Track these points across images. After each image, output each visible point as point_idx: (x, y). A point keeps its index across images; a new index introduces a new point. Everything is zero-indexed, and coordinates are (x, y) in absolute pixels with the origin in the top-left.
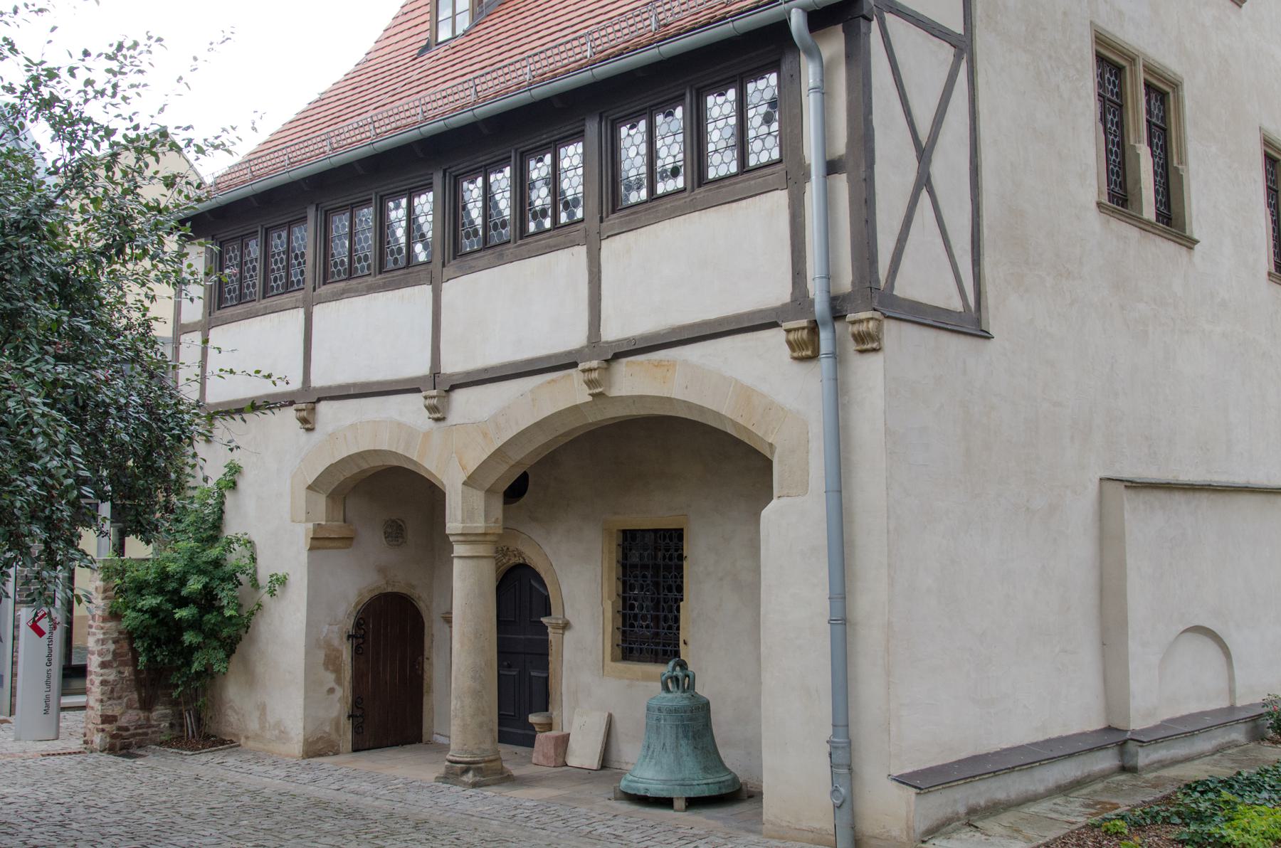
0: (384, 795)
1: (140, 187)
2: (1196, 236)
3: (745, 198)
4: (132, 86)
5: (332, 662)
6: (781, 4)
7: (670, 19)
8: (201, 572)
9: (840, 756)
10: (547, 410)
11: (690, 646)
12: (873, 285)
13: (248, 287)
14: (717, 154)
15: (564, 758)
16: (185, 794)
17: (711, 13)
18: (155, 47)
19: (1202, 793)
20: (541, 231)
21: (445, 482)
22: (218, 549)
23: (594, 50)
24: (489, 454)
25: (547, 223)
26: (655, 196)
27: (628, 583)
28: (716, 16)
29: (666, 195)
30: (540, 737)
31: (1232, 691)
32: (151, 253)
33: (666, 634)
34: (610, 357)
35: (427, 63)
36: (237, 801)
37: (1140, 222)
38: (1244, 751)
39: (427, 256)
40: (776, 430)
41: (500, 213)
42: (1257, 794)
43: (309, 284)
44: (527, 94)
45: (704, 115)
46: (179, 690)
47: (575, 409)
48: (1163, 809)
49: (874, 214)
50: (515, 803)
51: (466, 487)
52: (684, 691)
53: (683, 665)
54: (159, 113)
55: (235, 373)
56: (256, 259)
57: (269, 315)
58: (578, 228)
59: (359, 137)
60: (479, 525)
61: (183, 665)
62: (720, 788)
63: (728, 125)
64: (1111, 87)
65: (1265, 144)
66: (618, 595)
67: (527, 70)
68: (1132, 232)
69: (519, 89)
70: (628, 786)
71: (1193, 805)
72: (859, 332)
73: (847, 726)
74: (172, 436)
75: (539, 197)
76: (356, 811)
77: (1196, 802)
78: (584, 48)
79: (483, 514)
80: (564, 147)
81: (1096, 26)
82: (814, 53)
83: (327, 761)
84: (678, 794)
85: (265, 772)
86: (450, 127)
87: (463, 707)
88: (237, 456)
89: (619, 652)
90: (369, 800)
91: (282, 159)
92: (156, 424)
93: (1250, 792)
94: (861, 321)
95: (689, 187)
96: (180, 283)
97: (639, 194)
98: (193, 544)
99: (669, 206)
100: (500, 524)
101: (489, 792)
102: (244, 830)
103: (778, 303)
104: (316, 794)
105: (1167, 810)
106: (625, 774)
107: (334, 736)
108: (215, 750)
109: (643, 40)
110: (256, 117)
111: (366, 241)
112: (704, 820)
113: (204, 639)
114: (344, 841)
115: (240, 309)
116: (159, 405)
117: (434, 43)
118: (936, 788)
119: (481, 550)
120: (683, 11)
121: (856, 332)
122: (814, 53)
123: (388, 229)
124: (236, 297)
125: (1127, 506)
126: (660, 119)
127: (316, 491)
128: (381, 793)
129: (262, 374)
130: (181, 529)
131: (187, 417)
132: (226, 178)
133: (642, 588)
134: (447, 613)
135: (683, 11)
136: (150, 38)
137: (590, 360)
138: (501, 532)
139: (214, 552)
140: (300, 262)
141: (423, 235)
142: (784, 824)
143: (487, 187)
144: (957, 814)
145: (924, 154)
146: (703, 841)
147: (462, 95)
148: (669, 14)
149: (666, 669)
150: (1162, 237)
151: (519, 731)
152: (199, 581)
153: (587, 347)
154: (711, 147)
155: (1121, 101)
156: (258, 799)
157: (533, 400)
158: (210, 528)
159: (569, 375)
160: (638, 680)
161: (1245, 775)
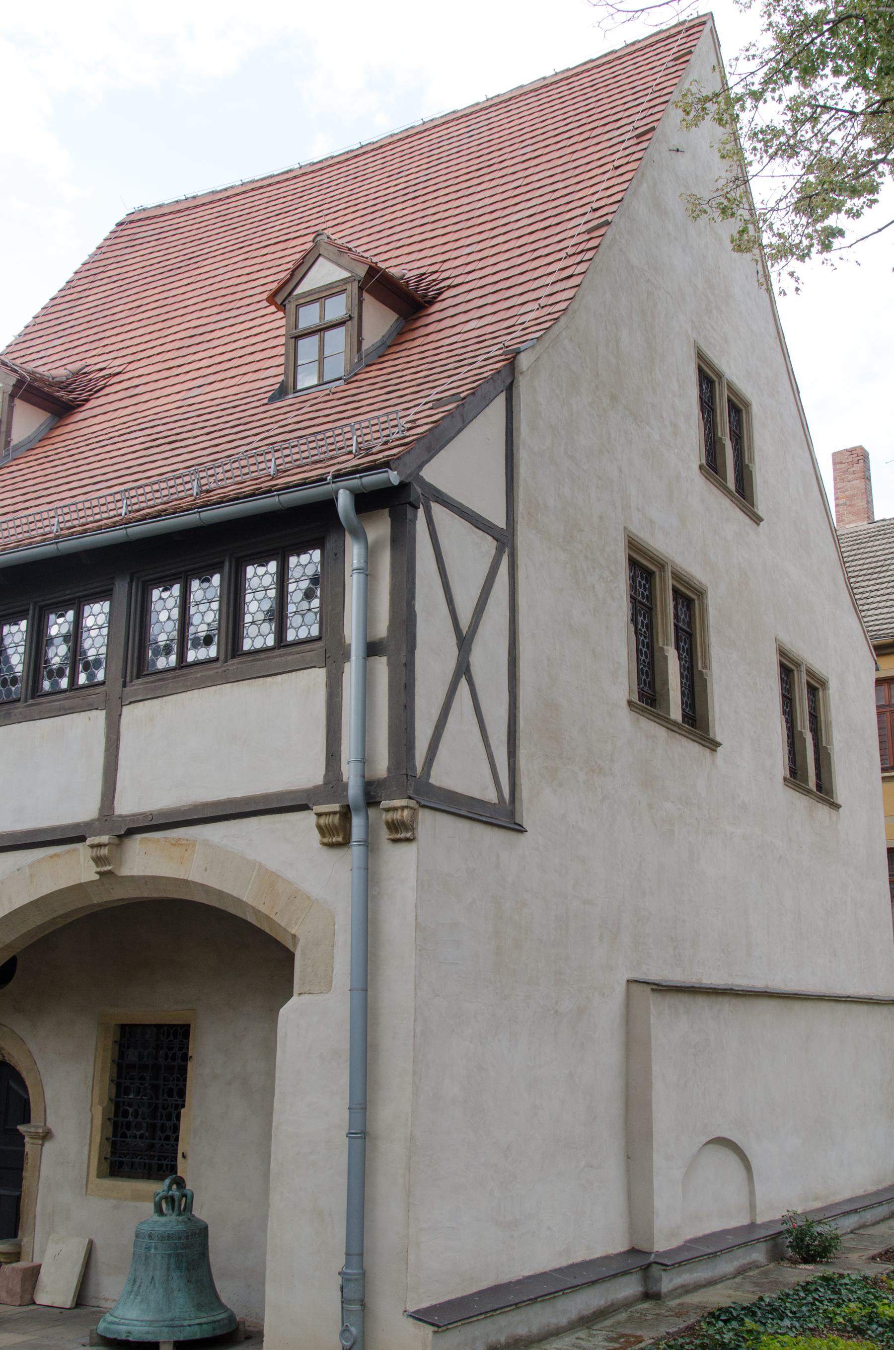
2: (719, 739)
3: (280, 674)
6: (329, 483)
7: (213, 486)
10: (46, 886)
12: (410, 773)
14: (254, 626)
15: (32, 1295)
17: (256, 484)
19: (726, 1322)
20: (56, 691)
23: (130, 508)
25: (64, 683)
26: (184, 664)
28: (261, 488)
29: (197, 664)
31: (752, 1206)
34: (122, 832)
37: (667, 722)
38: (766, 1274)
41: (11, 668)
42: (779, 1322)
44: (54, 547)
45: (243, 584)
47: (79, 888)
48: (688, 1341)
49: (414, 700)
52: (179, 1214)
53: (180, 1183)
58: (98, 691)
62: (214, 1329)
64: (641, 590)
65: (780, 654)
68: (660, 732)
69: (44, 540)
70: (106, 1329)
71: (717, 1337)
72: (393, 821)
73: (362, 1254)
75: (56, 655)
77: (720, 1332)
78: (119, 504)
80: (88, 604)
81: (630, 531)
82: (359, 534)
89: (106, 1166)
93: (772, 1319)
94: (395, 809)
95: (222, 658)
99: (199, 675)
103: (310, 785)
105: (692, 1342)
106: (105, 1313)
109: (184, 504)
118: (455, 1325)
120: (227, 479)
121: (390, 820)
122: (359, 534)
125: (653, 1009)
126: (195, 584)
133: (138, 1093)
135: (227, 479)
137: (100, 834)
145: (464, 642)
148: (212, 479)
149: (159, 1187)
150: (688, 738)
153: (98, 820)
154: (248, 618)
155: (651, 604)
157: (31, 876)
159: (75, 850)
160: (126, 1199)
161: (767, 1300)
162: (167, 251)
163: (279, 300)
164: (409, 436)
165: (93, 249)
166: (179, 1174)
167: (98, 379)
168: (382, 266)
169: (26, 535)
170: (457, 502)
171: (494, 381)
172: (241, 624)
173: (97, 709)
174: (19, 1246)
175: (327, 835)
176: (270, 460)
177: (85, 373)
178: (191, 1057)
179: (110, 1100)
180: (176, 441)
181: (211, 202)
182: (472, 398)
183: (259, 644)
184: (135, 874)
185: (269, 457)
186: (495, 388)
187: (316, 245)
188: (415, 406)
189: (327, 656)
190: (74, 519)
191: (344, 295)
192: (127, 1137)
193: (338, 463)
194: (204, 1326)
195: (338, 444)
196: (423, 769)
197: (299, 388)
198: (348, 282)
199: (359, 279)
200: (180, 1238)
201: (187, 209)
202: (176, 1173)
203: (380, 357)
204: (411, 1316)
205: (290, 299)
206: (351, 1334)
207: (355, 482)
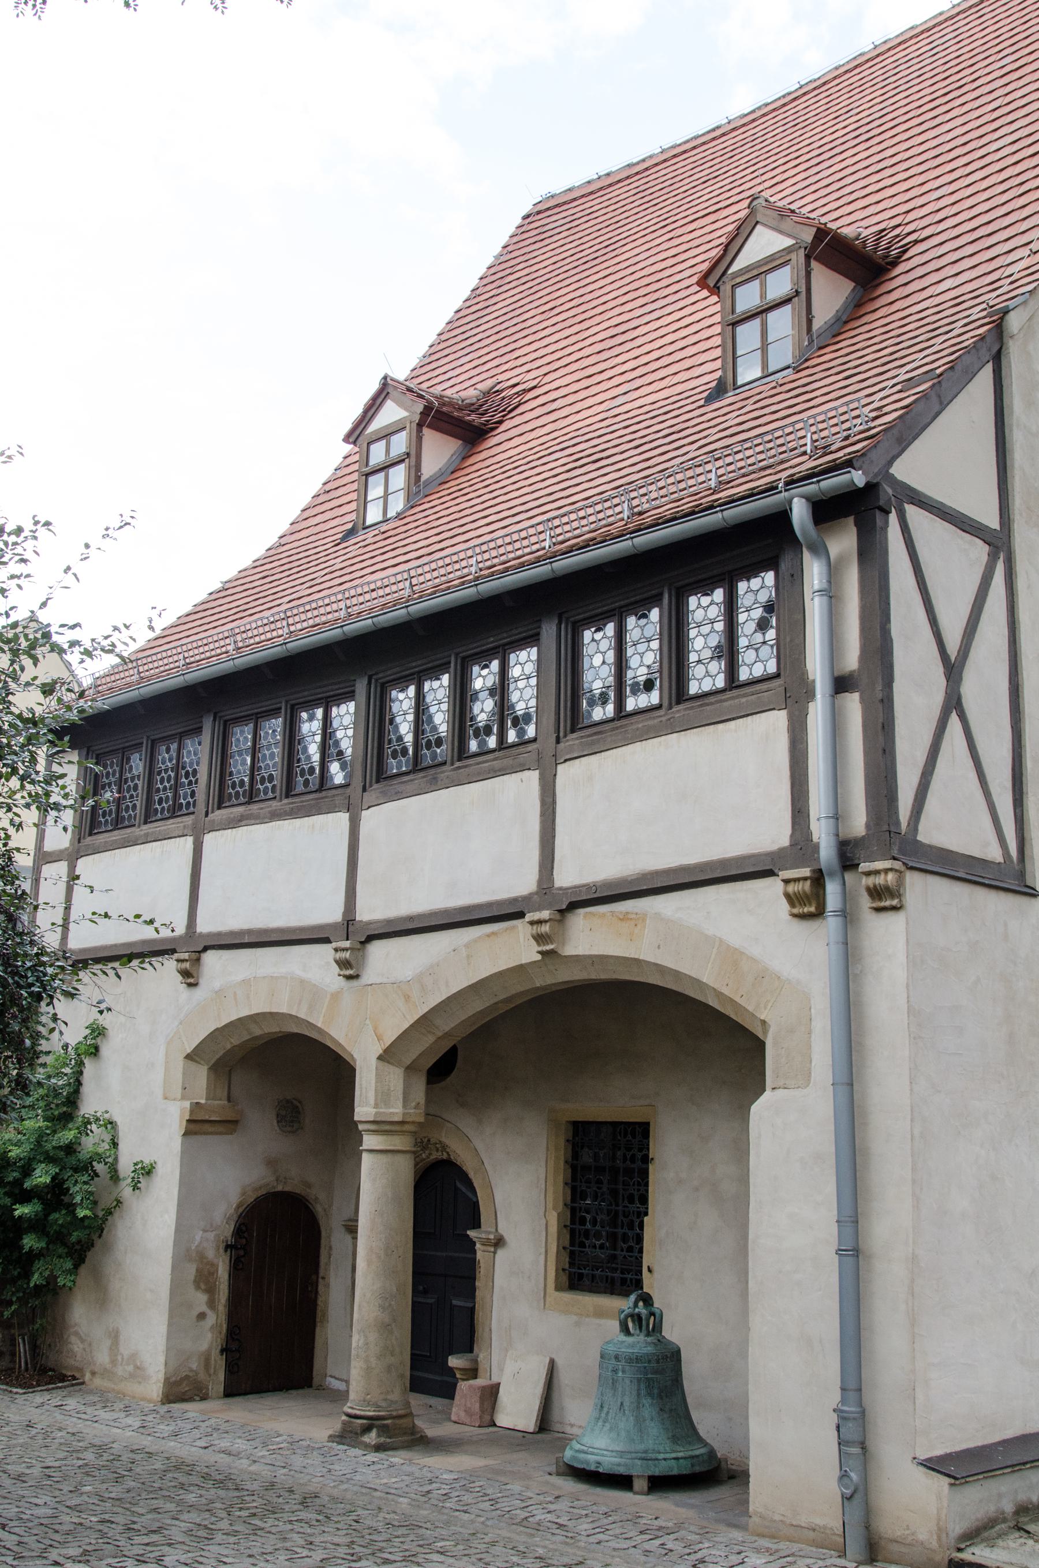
0: (263, 1457)
1: (12, 694)
3: (734, 719)
4: (12, 577)
5: (205, 1280)
6: (781, 492)
7: (646, 506)
8: (50, 1159)
9: (851, 1431)
10: (485, 969)
11: (656, 1274)
12: (893, 829)
13: (127, 810)
14: (700, 666)
16: (15, 1446)
18: (42, 532)
20: (484, 752)
22: (72, 1132)
23: (554, 540)
24: (412, 1022)
25: (492, 742)
26: (623, 714)
27: (579, 1190)
28: (701, 504)
30: (463, 1386)
32: (21, 772)
33: (625, 1257)
34: (564, 907)
35: (354, 551)
36: (78, 1459)
39: (345, 777)
40: (770, 1005)
41: (435, 728)
43: (201, 807)
44: (473, 590)
46: (13, 1308)
47: (520, 970)
50: (429, 1475)
51: (381, 1063)
52: (648, 1335)
53: (647, 1300)
54: (40, 608)
55: (110, 918)
56: (139, 776)
57: (151, 844)
59: (269, 635)
60: (396, 1111)
61: (19, 1277)
62: (693, 1465)
63: (715, 631)
66: (565, 1205)
67: (473, 561)
69: (463, 583)
70: (574, 1458)
72: (875, 886)
73: (860, 1390)
74: (31, 994)
76: (229, 1478)
78: (542, 537)
79: (401, 1097)
82: (819, 549)
83: (193, 1409)
84: (638, 1470)
85: (114, 1420)
86: (380, 626)
87: (367, 1344)
88: (106, 1020)
89: (565, 1279)
90: (244, 1463)
91: (176, 658)
92: (13, 978)
94: (877, 872)
95: (666, 704)
96: (45, 808)
97: (604, 710)
98: (41, 1123)
99: (640, 726)
100: (422, 1111)
101: (397, 1458)
102: (87, 1499)
103: (775, 847)
104: (177, 1453)
106: (571, 1440)
107: (202, 1376)
108: (53, 1389)
109: (614, 530)
110: (154, 614)
111: (272, 755)
112: (673, 1507)
113: (48, 1244)
114: (214, 1519)
115: (117, 835)
116: (17, 955)
117: (361, 526)
118: (976, 1478)
120: (662, 497)
121: (872, 886)
122: (819, 549)
123: (299, 744)
124: (112, 820)
126: (631, 621)
127: (196, 1062)
128: (261, 1454)
129: (142, 919)
130: (27, 1103)
131: (50, 970)
132: (108, 679)
133: (595, 1198)
134: (350, 1220)
135: (662, 497)
136: (36, 523)
137: (540, 909)
138: (422, 1120)
139: (67, 1135)
140: (191, 781)
141: (340, 753)
142: (777, 1517)
143: (420, 697)
144: (1003, 1513)
146: (672, 1536)
147: (394, 588)
148: (644, 499)
149: (625, 1304)
151: (438, 1378)
152: (47, 1172)
153: (537, 893)
154: (693, 657)
156: (106, 1456)
157: (468, 957)
158: (63, 1104)
159: (514, 927)
160: (588, 1316)
163: (711, 282)
164: (874, 427)
165: (498, 249)
167: (511, 397)
169: (444, 579)
171: (978, 350)
173: (529, 769)
175: (797, 904)
176: (710, 471)
177: (497, 391)
178: (652, 1159)
181: (628, 178)
182: (950, 373)
183: (707, 686)
184: (581, 954)
185: (708, 467)
188: (880, 391)
189: (788, 695)
190: (493, 557)
191: (789, 266)
192: (585, 1247)
194: (681, 1461)
195: (790, 445)
196: (909, 824)
199: (806, 245)
200: (649, 1362)
201: (601, 189)
202: (642, 1288)
203: (835, 336)
204: (921, 1464)
205: (724, 279)
206: (852, 1480)
207: (811, 488)
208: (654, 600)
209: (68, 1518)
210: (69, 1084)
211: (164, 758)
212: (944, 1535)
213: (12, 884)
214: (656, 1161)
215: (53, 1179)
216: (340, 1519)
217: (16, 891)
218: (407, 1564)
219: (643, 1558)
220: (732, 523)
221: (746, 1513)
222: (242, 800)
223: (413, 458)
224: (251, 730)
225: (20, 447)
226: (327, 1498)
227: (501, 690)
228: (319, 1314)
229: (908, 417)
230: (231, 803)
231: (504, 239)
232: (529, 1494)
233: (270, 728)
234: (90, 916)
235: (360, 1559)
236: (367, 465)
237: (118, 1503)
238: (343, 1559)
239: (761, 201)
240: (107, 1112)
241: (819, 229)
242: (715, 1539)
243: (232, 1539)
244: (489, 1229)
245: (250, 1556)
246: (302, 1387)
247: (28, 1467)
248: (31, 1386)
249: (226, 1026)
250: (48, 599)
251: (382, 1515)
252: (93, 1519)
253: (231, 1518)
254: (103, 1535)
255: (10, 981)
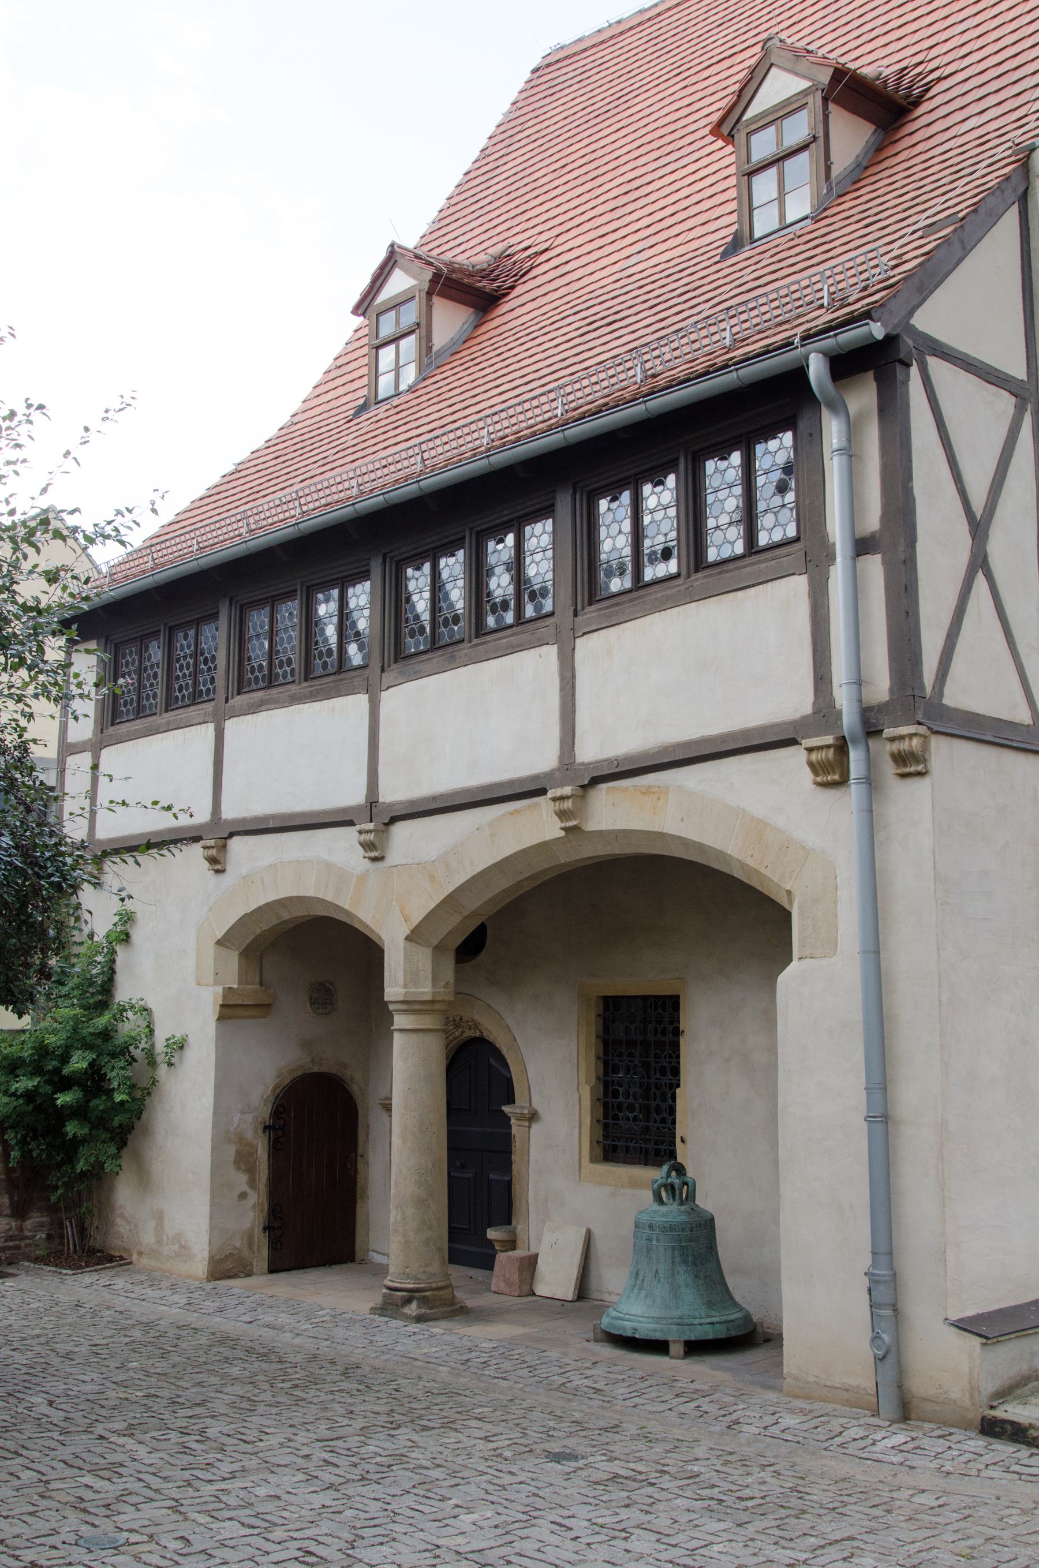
0: (306, 1330)
1: (16, 583)
3: (753, 586)
4: (8, 463)
5: (244, 1160)
6: (797, 348)
7: (659, 368)
8: (87, 1046)
9: (883, 1294)
10: (508, 847)
12: (917, 693)
13: (148, 698)
16: (64, 1325)
18: (36, 416)
21: (383, 937)
23: (566, 407)
24: (438, 902)
25: (509, 618)
26: (641, 584)
28: (715, 364)
29: (656, 582)
30: (501, 1258)
34: (586, 782)
36: (126, 1336)
39: (363, 659)
41: (451, 605)
43: (221, 694)
44: (485, 462)
50: (469, 1344)
51: (409, 944)
52: (682, 1203)
53: (680, 1170)
54: (41, 494)
55: (127, 805)
56: (158, 664)
58: (547, 623)
59: (281, 517)
60: (425, 990)
62: (728, 1330)
67: (484, 432)
70: (609, 1324)
73: (891, 1253)
75: (499, 586)
78: (554, 405)
79: (430, 977)
80: (529, 524)
82: (838, 407)
83: (237, 1285)
84: (675, 1336)
85: (161, 1298)
89: (599, 1151)
91: (189, 543)
92: (32, 869)
94: (901, 738)
95: (684, 572)
101: (437, 1328)
102: (133, 1375)
103: (797, 716)
106: (608, 1307)
107: (246, 1253)
108: (102, 1269)
109: (627, 395)
110: (156, 496)
113: (91, 1130)
114: (257, 1391)
115: (138, 725)
116: (36, 845)
117: (373, 401)
118: (1008, 1337)
119: (427, 1021)
122: (838, 407)
123: (316, 625)
126: (647, 489)
128: (304, 1327)
129: (160, 805)
130: (63, 993)
131: (69, 860)
132: (123, 567)
133: (628, 1071)
136: (29, 406)
137: (561, 785)
139: (102, 1021)
140: (210, 668)
142: (811, 1379)
143: (435, 574)
146: (707, 1399)
147: (406, 463)
148: (657, 362)
149: (657, 1174)
151: (476, 1250)
152: (84, 1058)
153: (558, 769)
156: (152, 1333)
157: (492, 835)
158: (98, 993)
159: (537, 804)
160: (623, 1186)
162: (592, 94)
163: (725, 130)
164: (894, 276)
165: (507, 106)
166: (679, 1160)
167: (523, 261)
168: (852, 66)
169: (455, 451)
170: (961, 352)
171: (1003, 192)
172: (704, 530)
174: (514, 1233)
175: (821, 772)
176: (724, 330)
177: (509, 255)
179: (598, 1078)
180: (616, 321)
181: (639, 24)
182: (973, 216)
183: (726, 553)
184: (604, 829)
185: (723, 325)
186: (1004, 200)
187: (766, 52)
188: (900, 238)
190: (503, 427)
191: (805, 111)
193: (808, 321)
195: (806, 299)
196: (934, 688)
197: (757, 235)
198: (809, 94)
199: (823, 87)
201: (612, 38)
202: (676, 1158)
203: (854, 183)
205: (738, 126)
207: (828, 342)
208: (670, 466)
209: (114, 1394)
210: (103, 973)
211: (182, 645)
212: (977, 1393)
213: (30, 775)
214: (687, 1034)
215: (91, 1065)
216: (380, 1388)
217: (34, 782)
218: (445, 1430)
219: (679, 1421)
220: (748, 382)
221: (780, 1375)
222: (261, 684)
223: (423, 328)
224: (268, 614)
225: (11, 328)
226: (368, 1369)
227: (517, 565)
228: (359, 1192)
229: (930, 263)
230: (251, 688)
231: (513, 96)
232: (567, 1361)
233: (286, 611)
234: (108, 805)
235: (399, 1427)
236: (377, 337)
237: (163, 1377)
238: (383, 1427)
239: (775, 41)
240: (142, 1000)
241: (836, 69)
242: (751, 1401)
243: (274, 1410)
244: (523, 1104)
245: (291, 1426)
246: (346, 1262)
247: (76, 1346)
248: (80, 1267)
249: (254, 911)
250: (48, 485)
251: (422, 1383)
252: (139, 1394)
253: (274, 1389)
254: (148, 1408)
255: (30, 872)
